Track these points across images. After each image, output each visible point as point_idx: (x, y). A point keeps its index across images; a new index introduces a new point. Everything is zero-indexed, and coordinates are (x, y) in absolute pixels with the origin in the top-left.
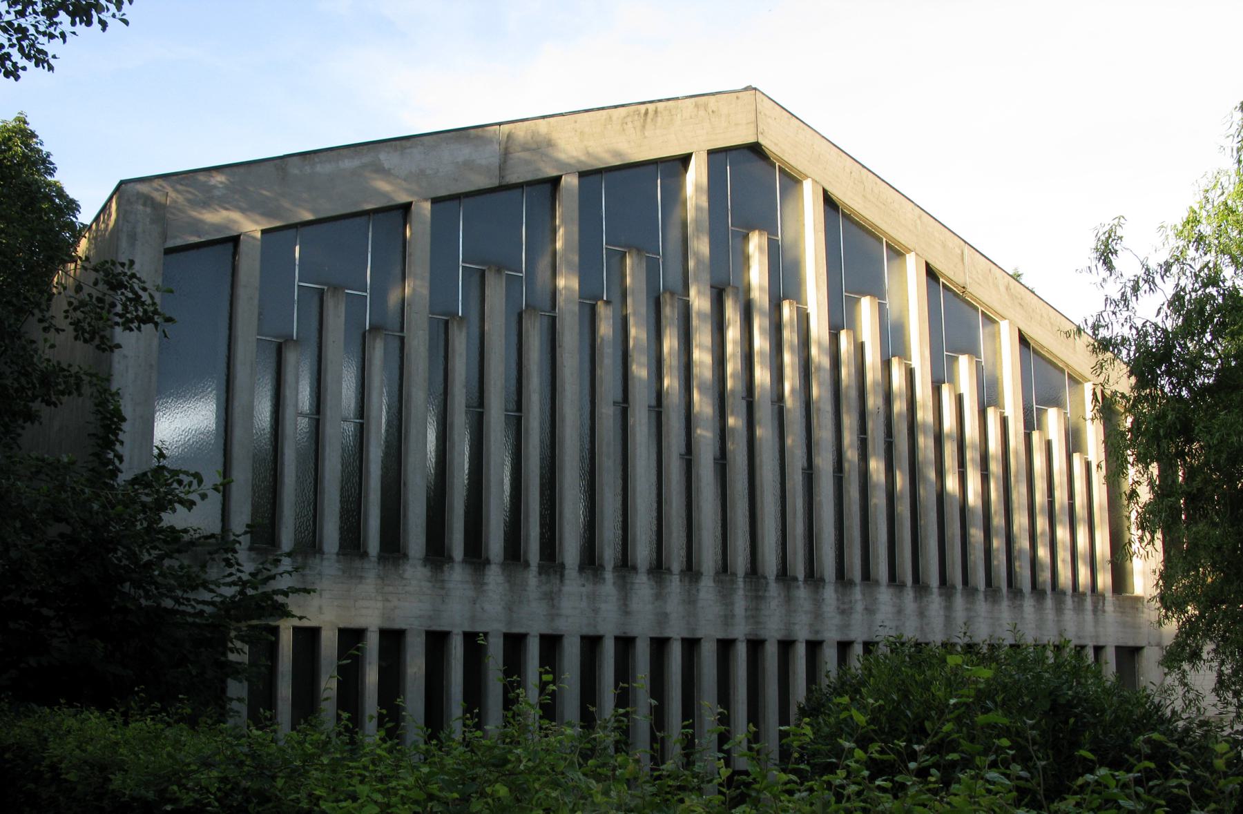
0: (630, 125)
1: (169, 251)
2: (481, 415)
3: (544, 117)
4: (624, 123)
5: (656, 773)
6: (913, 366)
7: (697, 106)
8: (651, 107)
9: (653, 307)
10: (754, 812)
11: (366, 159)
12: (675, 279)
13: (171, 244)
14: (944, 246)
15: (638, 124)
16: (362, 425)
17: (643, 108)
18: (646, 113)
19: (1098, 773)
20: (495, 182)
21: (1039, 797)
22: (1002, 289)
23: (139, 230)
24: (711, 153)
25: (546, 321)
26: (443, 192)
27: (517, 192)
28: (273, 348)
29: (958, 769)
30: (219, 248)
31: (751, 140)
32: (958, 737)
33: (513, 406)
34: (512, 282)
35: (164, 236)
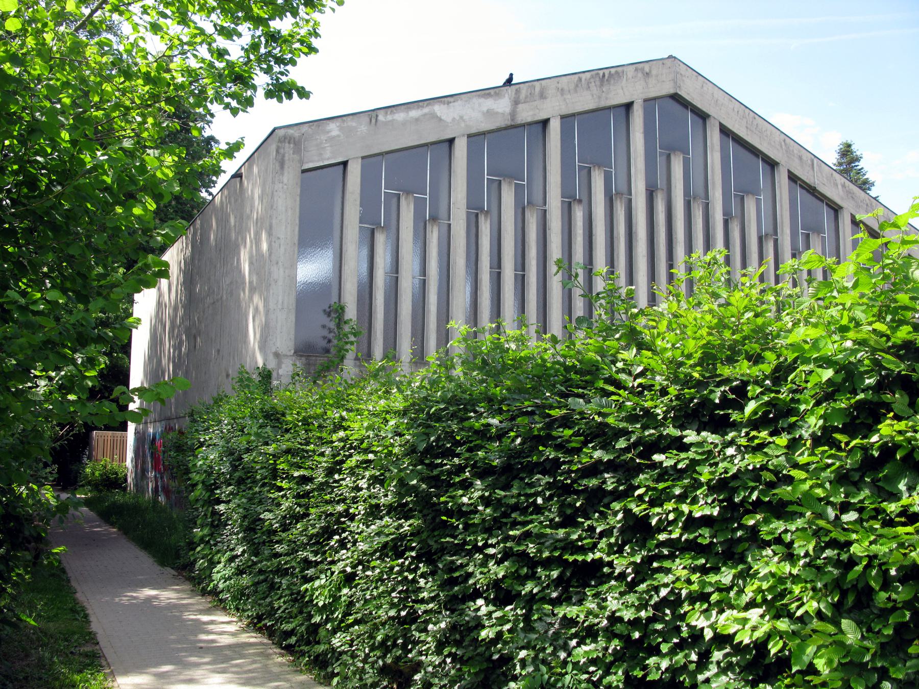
0: (593, 84)
1: (304, 171)
2: (499, 274)
3: (538, 80)
4: (589, 83)
5: (588, 377)
6: (837, 156)
7: (636, 70)
8: (607, 72)
9: (608, 203)
10: (916, 642)
11: (426, 110)
12: (623, 188)
13: (306, 166)
14: (800, 158)
15: (598, 83)
16: (424, 280)
17: (601, 72)
18: (604, 75)
19: (665, 507)
20: (509, 123)
21: (451, 490)
22: (840, 187)
23: (286, 158)
24: (645, 101)
25: (540, 213)
26: (474, 131)
27: (521, 129)
28: (369, 232)
29: (118, 497)
30: (335, 168)
31: (672, 91)
32: (811, 487)
33: (520, 267)
34: (519, 189)
35: (302, 162)
